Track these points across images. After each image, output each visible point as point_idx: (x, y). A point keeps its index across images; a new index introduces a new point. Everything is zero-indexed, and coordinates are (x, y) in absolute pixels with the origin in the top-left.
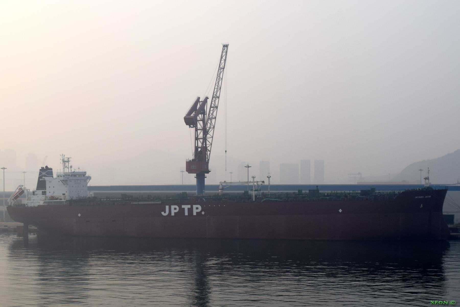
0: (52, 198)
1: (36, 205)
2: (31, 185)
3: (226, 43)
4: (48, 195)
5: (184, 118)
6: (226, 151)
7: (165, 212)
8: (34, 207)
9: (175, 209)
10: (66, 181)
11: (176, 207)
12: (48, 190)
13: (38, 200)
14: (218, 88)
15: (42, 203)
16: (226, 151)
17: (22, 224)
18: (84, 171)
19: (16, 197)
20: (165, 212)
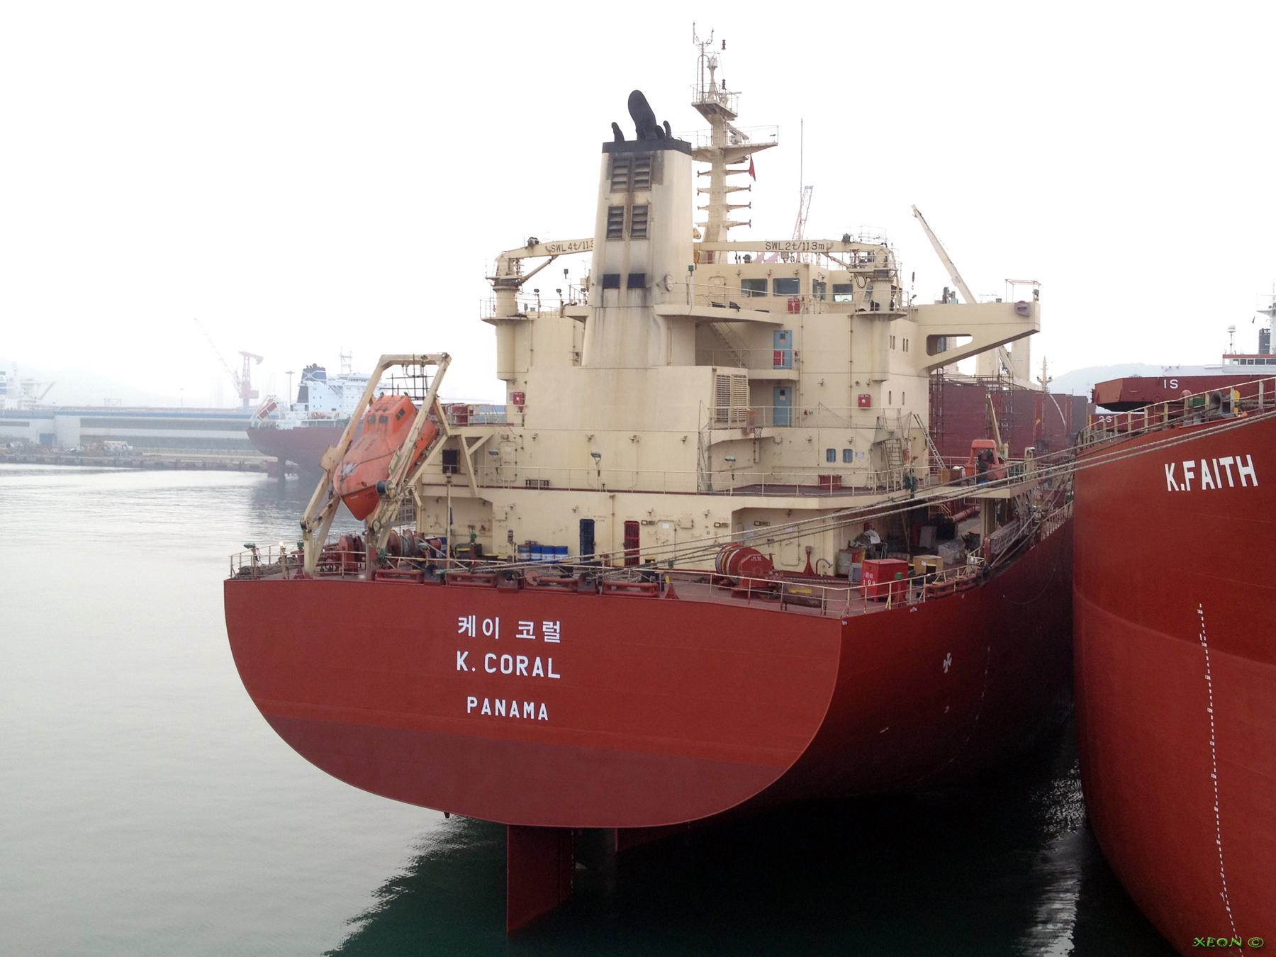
0: (316, 416)
1: (291, 427)
2: (286, 393)
3: (590, 434)
4: (311, 409)
5: (226, 583)
6: (566, 272)
7: (490, 659)
8: (289, 431)
9: (522, 662)
10: (340, 387)
11: (525, 658)
12: (311, 402)
13: (292, 420)
14: (948, 262)
15: (298, 424)
16: (566, 272)
17: (274, 459)
18: (734, 111)
19: (264, 415)
20: (490, 659)
